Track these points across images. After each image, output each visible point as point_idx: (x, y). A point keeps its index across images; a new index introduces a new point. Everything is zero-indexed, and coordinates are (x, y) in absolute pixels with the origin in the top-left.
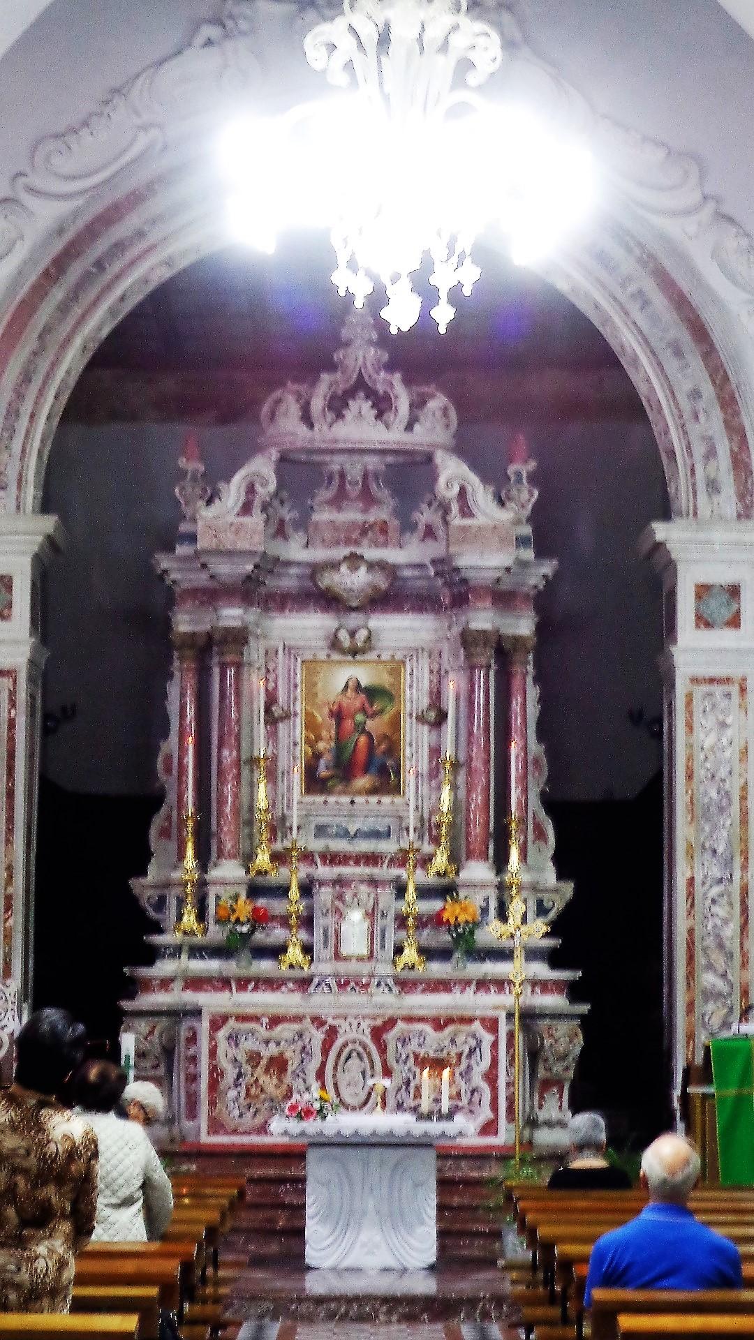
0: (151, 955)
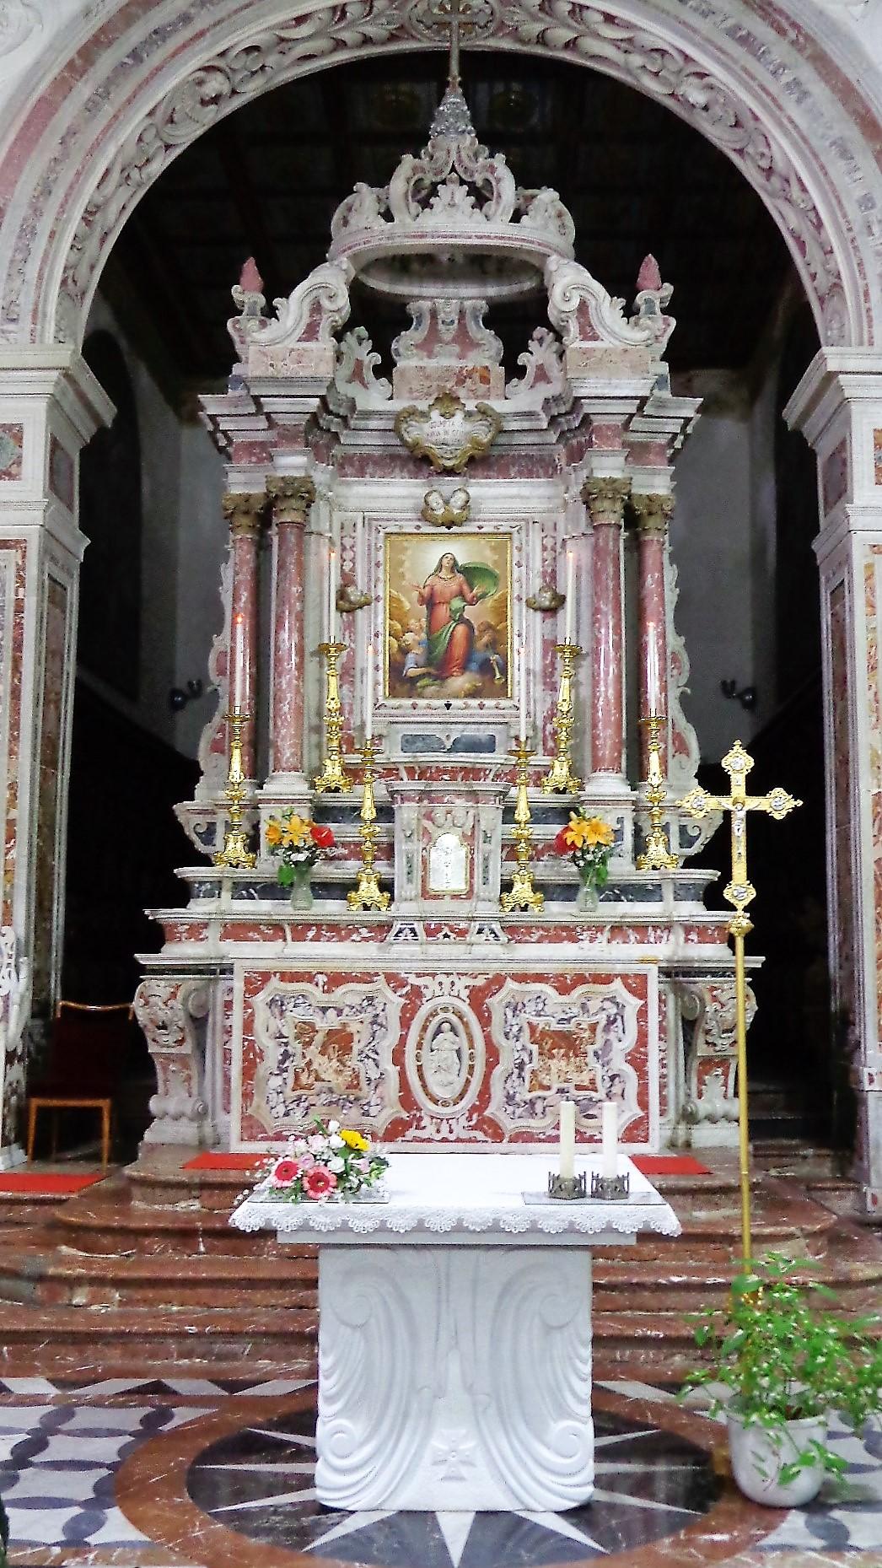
0: (181, 894)
